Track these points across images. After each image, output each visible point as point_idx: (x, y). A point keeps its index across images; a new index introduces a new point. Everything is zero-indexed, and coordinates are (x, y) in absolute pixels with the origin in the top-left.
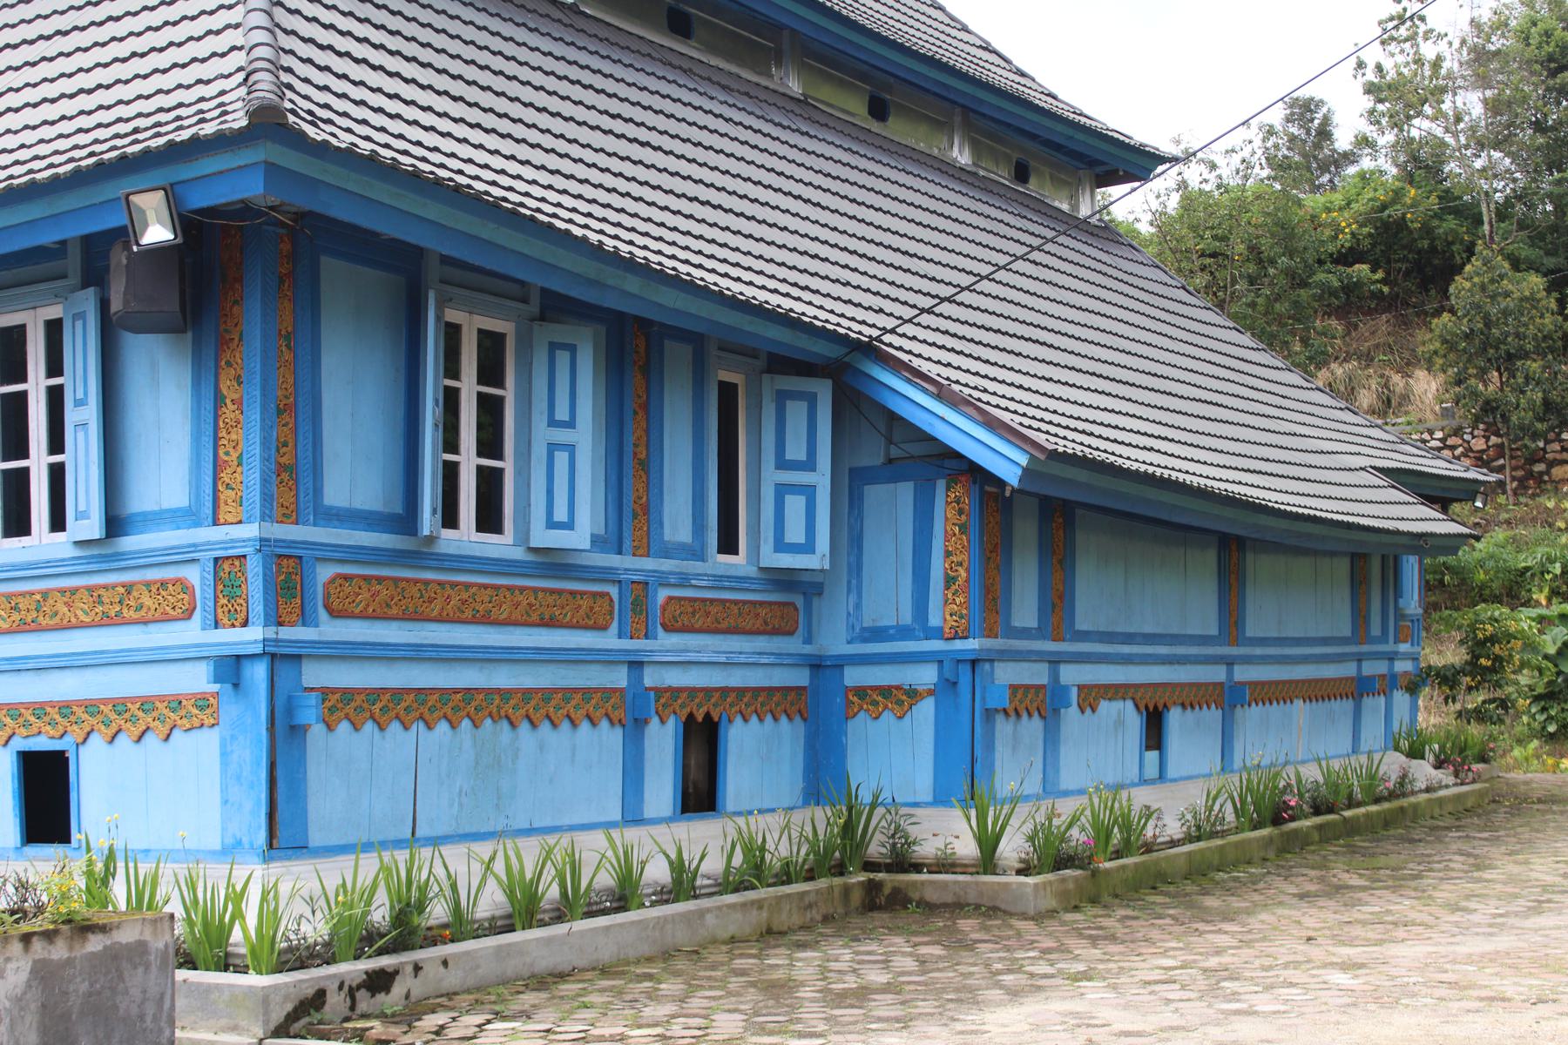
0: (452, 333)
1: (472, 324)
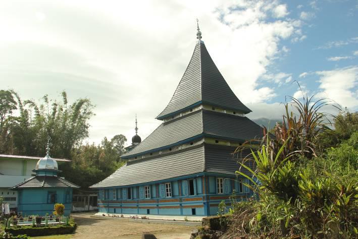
0: (218, 180)
1: (219, 179)
